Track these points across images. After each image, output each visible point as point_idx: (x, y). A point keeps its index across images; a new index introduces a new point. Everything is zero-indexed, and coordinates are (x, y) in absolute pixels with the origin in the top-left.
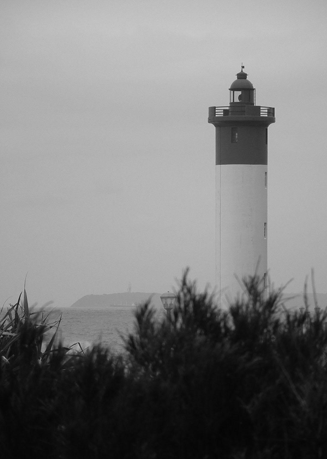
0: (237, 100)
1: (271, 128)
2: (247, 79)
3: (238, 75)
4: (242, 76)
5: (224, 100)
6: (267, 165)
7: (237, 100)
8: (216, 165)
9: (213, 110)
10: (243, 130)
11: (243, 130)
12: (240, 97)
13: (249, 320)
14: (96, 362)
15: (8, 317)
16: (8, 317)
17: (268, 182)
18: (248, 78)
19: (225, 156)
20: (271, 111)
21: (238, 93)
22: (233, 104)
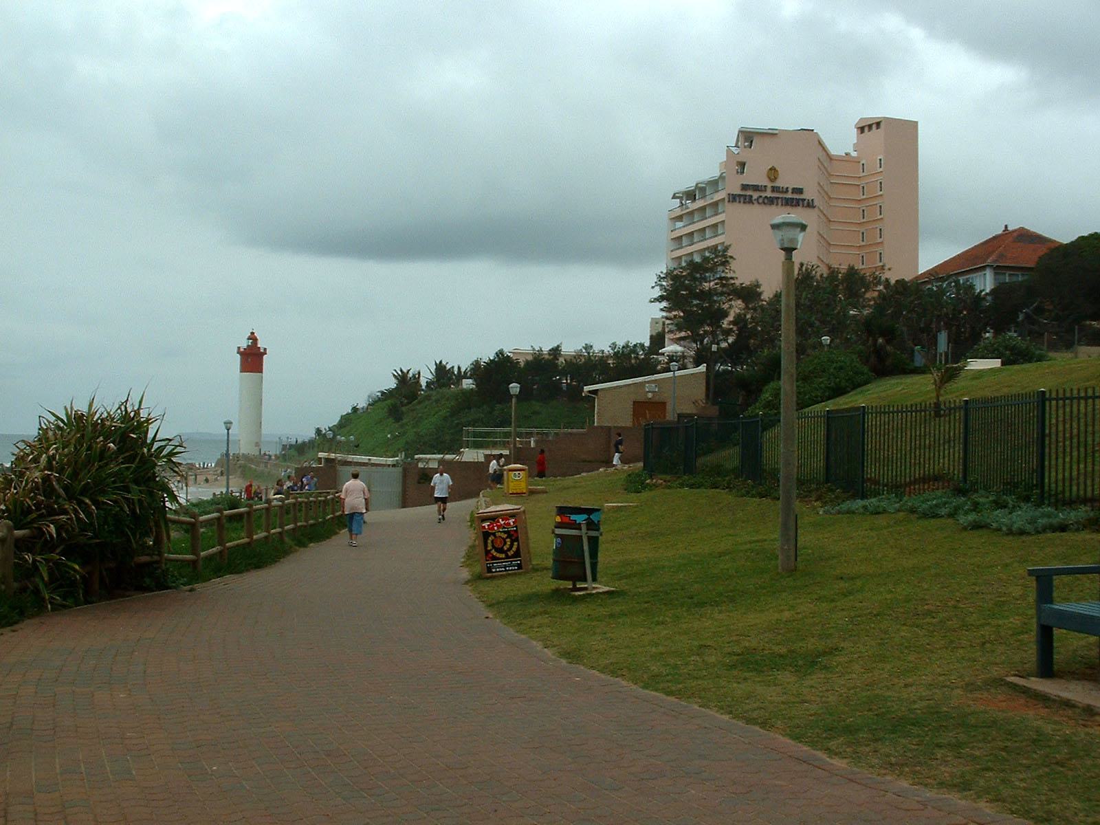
0: (250, 344)
1: (265, 357)
2: (1034, 578)
3: (402, 378)
4: (252, 333)
5: (244, 344)
6: (262, 372)
7: (250, 344)
8: (241, 372)
9: (239, 348)
10: (252, 358)
11: (252, 358)
12: (251, 343)
13: (423, 382)
14: (531, 361)
15: (119, 411)
16: (119, 411)
17: (704, 389)
18: (255, 334)
19: (244, 368)
20: (265, 349)
21: (251, 341)
22: (248, 346)
